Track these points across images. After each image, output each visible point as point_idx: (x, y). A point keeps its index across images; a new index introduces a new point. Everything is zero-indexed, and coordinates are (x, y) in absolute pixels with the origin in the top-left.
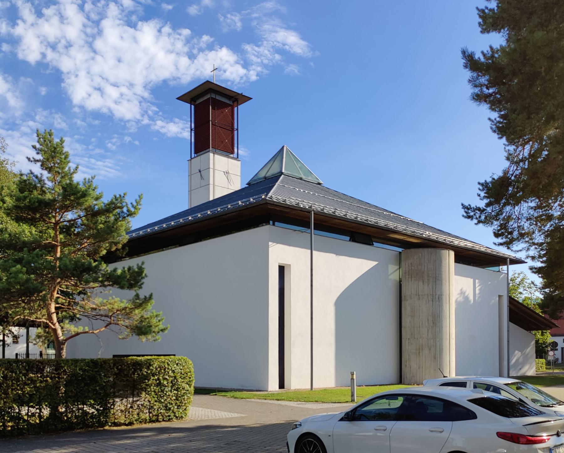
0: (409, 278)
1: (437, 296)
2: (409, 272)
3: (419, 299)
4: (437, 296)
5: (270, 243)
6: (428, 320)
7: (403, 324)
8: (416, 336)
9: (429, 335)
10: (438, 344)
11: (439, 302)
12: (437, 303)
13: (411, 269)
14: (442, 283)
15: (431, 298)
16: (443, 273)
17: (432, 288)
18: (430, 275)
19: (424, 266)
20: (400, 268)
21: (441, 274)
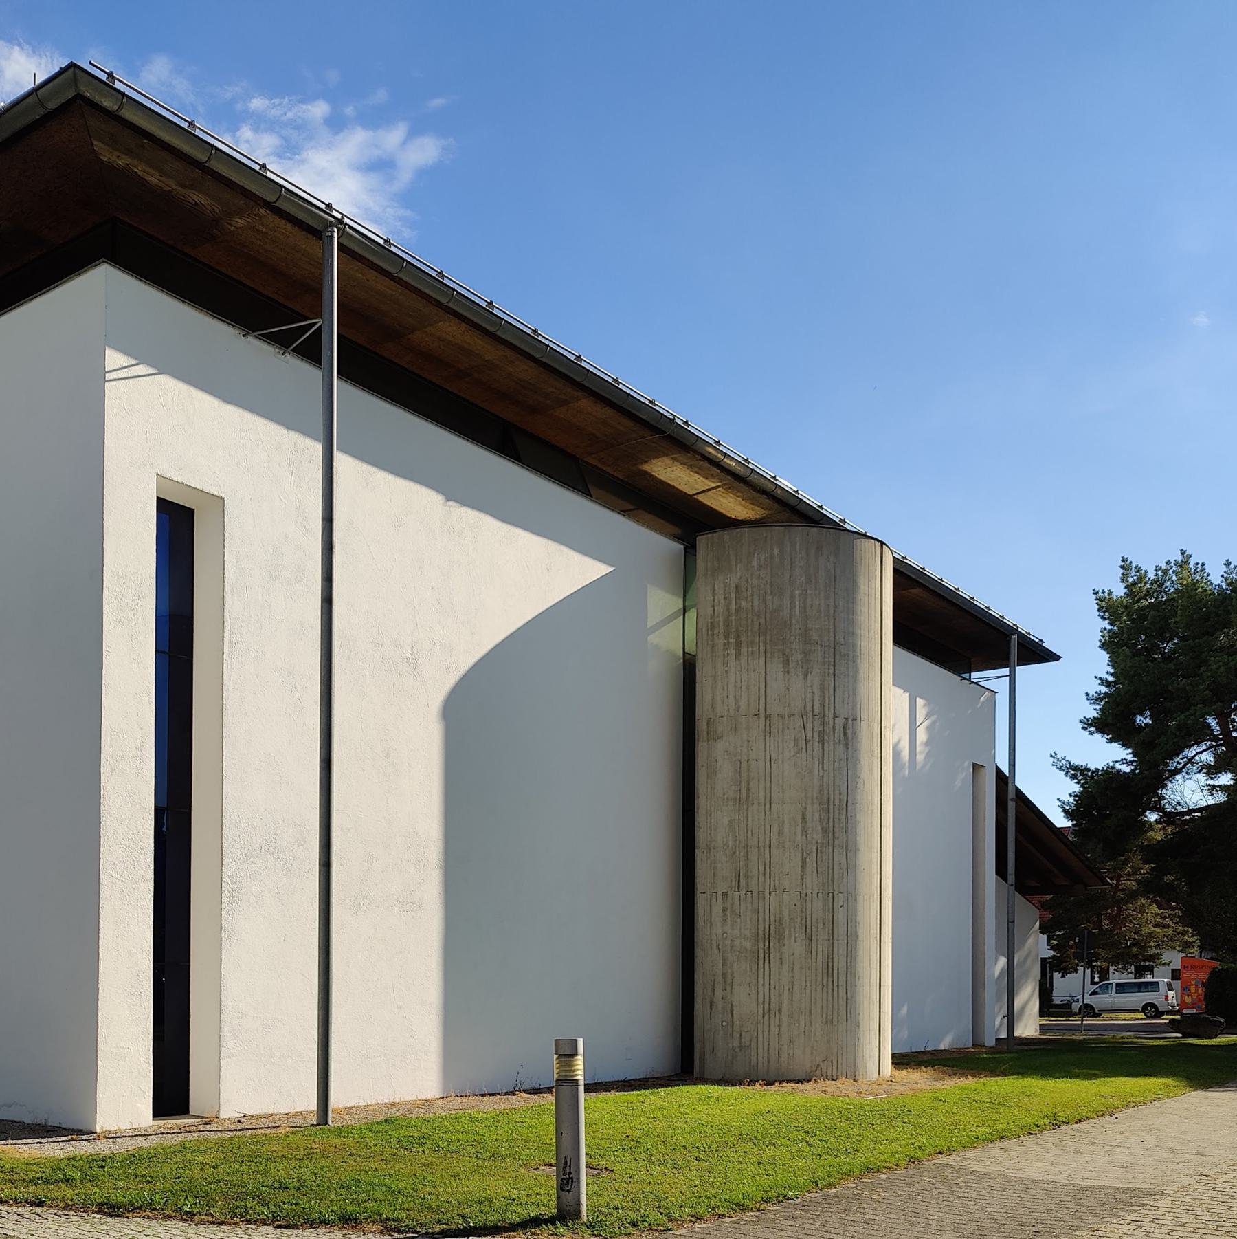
0: (726, 646)
1: (840, 722)
2: (727, 623)
3: (768, 731)
4: (840, 722)
5: (114, 359)
6: (804, 818)
7: (701, 835)
8: (754, 885)
9: (808, 880)
10: (841, 916)
11: (847, 746)
12: (840, 749)
13: (737, 611)
14: (856, 671)
15: (818, 728)
16: (862, 632)
17: (822, 689)
18: (815, 637)
19: (792, 597)
20: (685, 611)
21: (854, 634)
